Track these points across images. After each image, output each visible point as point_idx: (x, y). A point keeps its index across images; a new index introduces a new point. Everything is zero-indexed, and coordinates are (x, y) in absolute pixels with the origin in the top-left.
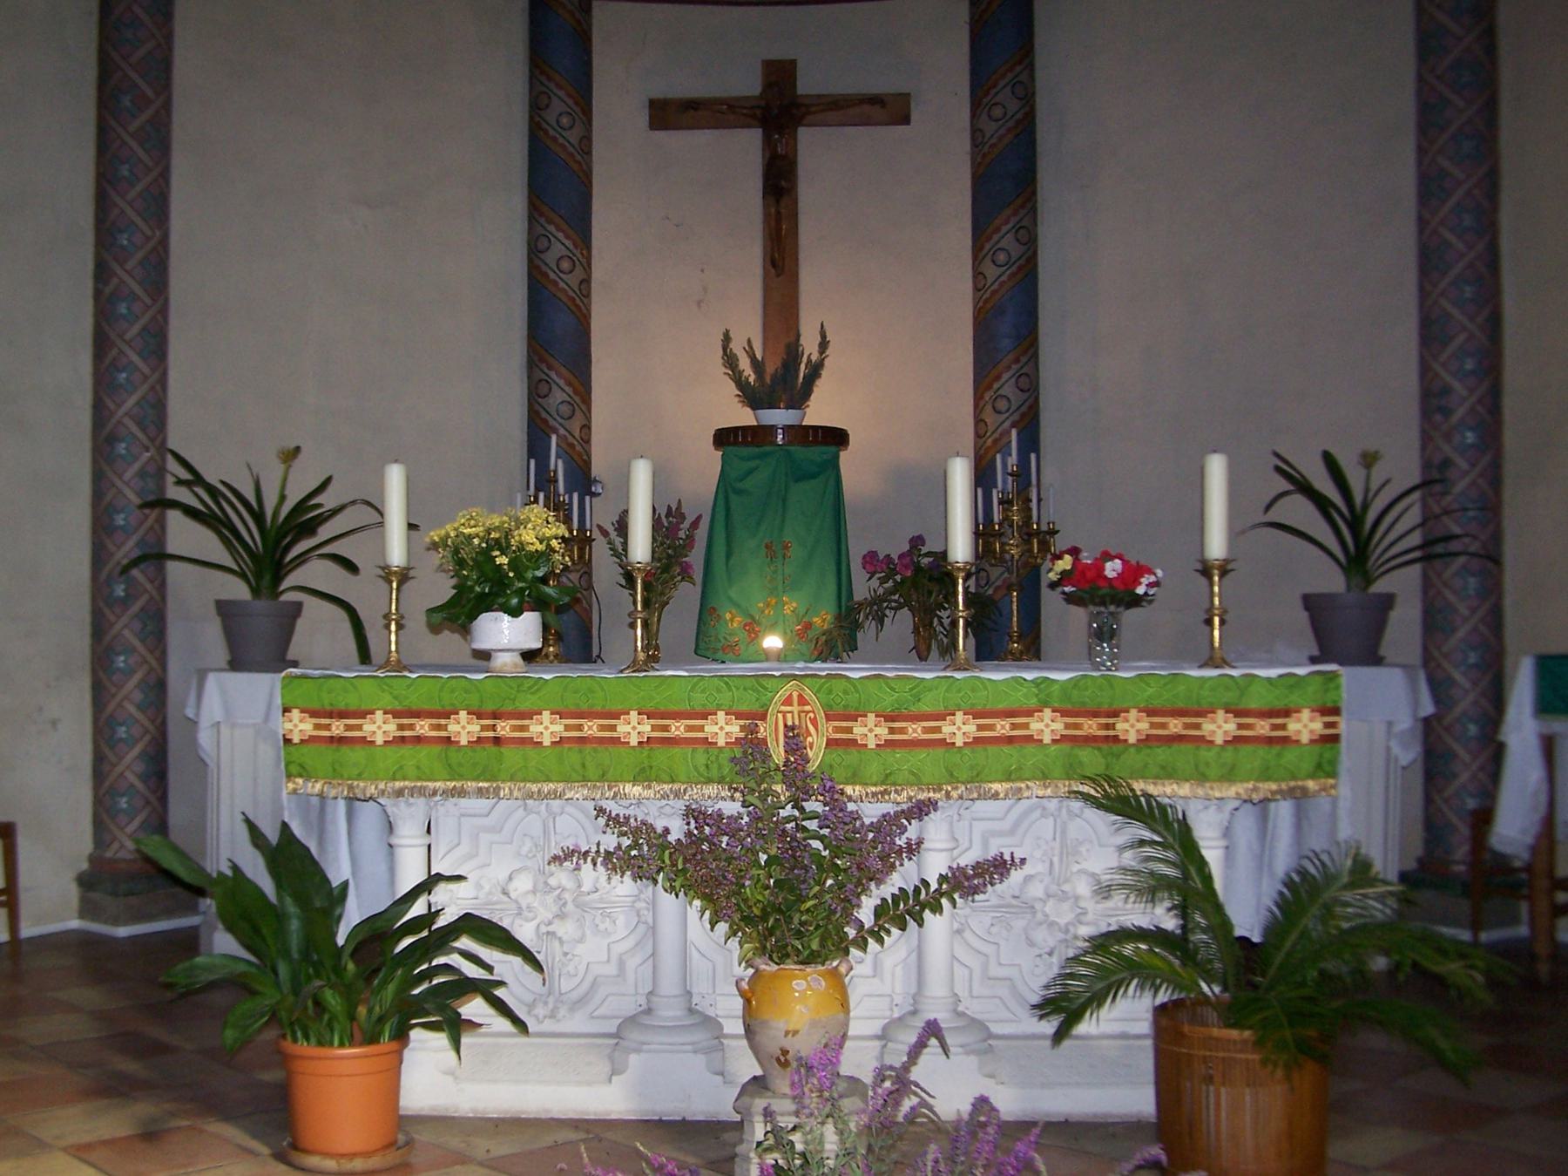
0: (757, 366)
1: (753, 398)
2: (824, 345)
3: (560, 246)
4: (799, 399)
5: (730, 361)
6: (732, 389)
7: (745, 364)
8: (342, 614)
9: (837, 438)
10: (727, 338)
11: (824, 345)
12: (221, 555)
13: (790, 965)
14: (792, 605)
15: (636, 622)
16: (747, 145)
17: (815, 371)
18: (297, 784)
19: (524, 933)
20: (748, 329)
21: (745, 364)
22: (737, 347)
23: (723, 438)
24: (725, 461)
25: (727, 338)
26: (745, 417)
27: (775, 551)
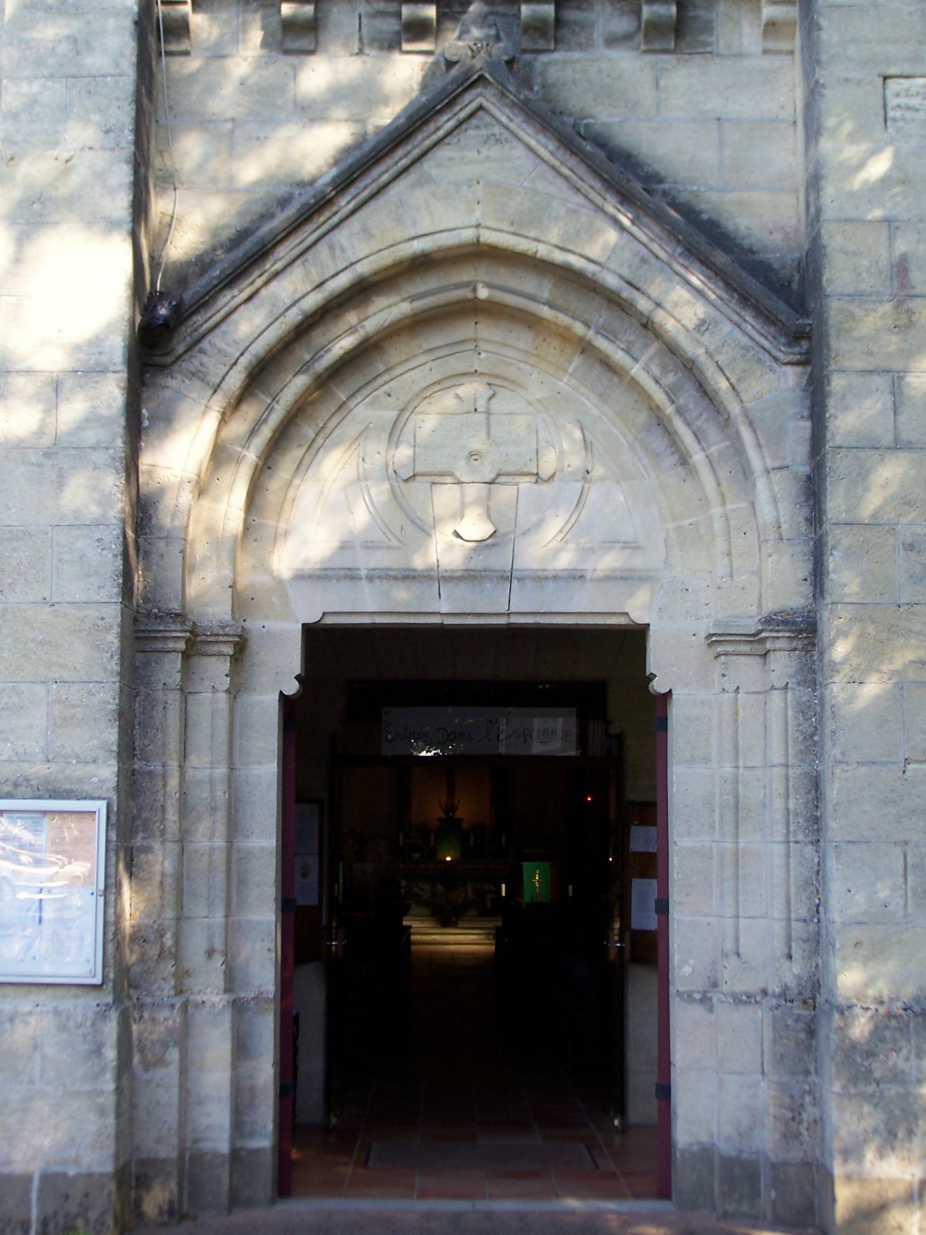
4: (454, 813)
5: (441, 805)
17: (457, 807)
23: (439, 819)
26: (444, 816)
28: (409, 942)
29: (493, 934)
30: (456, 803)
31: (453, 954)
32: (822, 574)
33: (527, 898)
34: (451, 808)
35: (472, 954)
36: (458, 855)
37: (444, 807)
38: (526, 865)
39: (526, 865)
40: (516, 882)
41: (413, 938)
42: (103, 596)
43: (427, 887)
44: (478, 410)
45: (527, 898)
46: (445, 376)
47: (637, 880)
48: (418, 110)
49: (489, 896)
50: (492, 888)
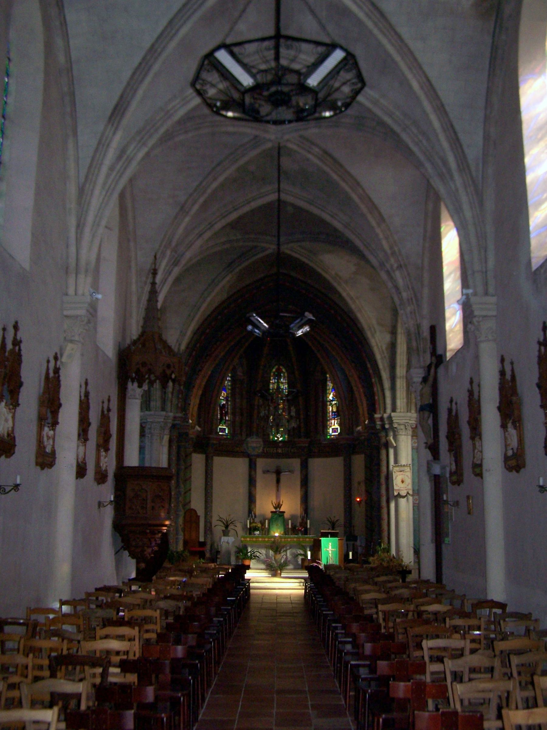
0: (275, 505)
1: (275, 508)
2: (282, 502)
3: (253, 473)
4: (280, 508)
5: (272, 504)
6: (272, 507)
7: (274, 504)
8: (235, 531)
9: (284, 512)
10: (272, 501)
11: (282, 502)
12: (223, 525)
13: (165, 609)
14: (279, 531)
15: (265, 522)
16: (274, 476)
17: (282, 505)
18: (439, 702)
19: (217, 524)
20: (274, 501)
21: (274, 504)
22: (273, 502)
23: (272, 512)
24: (272, 515)
25: (272, 501)
26: (274, 510)
27: (277, 525)
28: (249, 588)
29: (303, 583)
30: (281, 503)
31: (277, 596)
32: (391, 378)
33: (324, 561)
34: (278, 506)
35: (290, 596)
36: (282, 532)
37: (275, 505)
38: (323, 540)
39: (323, 540)
40: (316, 547)
41: (251, 585)
42: (130, 400)
43: (263, 551)
44: (77, 642)
45: (324, 561)
46: (75, 284)
47: (441, 670)
48: (345, 474)
49: (300, 558)
50: (302, 552)
